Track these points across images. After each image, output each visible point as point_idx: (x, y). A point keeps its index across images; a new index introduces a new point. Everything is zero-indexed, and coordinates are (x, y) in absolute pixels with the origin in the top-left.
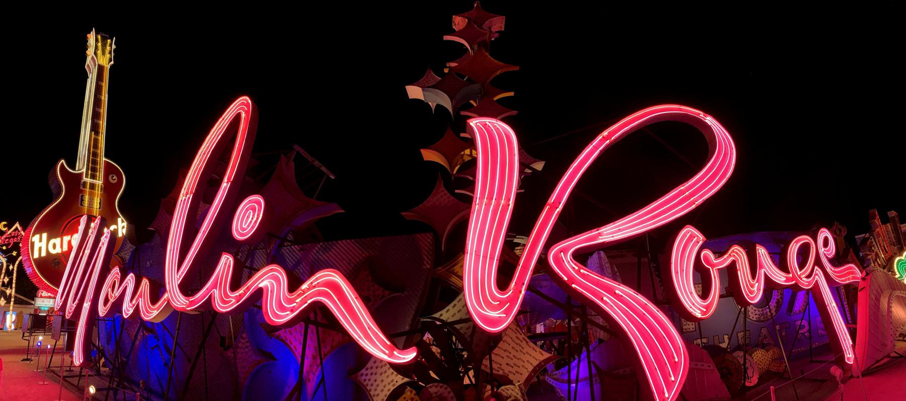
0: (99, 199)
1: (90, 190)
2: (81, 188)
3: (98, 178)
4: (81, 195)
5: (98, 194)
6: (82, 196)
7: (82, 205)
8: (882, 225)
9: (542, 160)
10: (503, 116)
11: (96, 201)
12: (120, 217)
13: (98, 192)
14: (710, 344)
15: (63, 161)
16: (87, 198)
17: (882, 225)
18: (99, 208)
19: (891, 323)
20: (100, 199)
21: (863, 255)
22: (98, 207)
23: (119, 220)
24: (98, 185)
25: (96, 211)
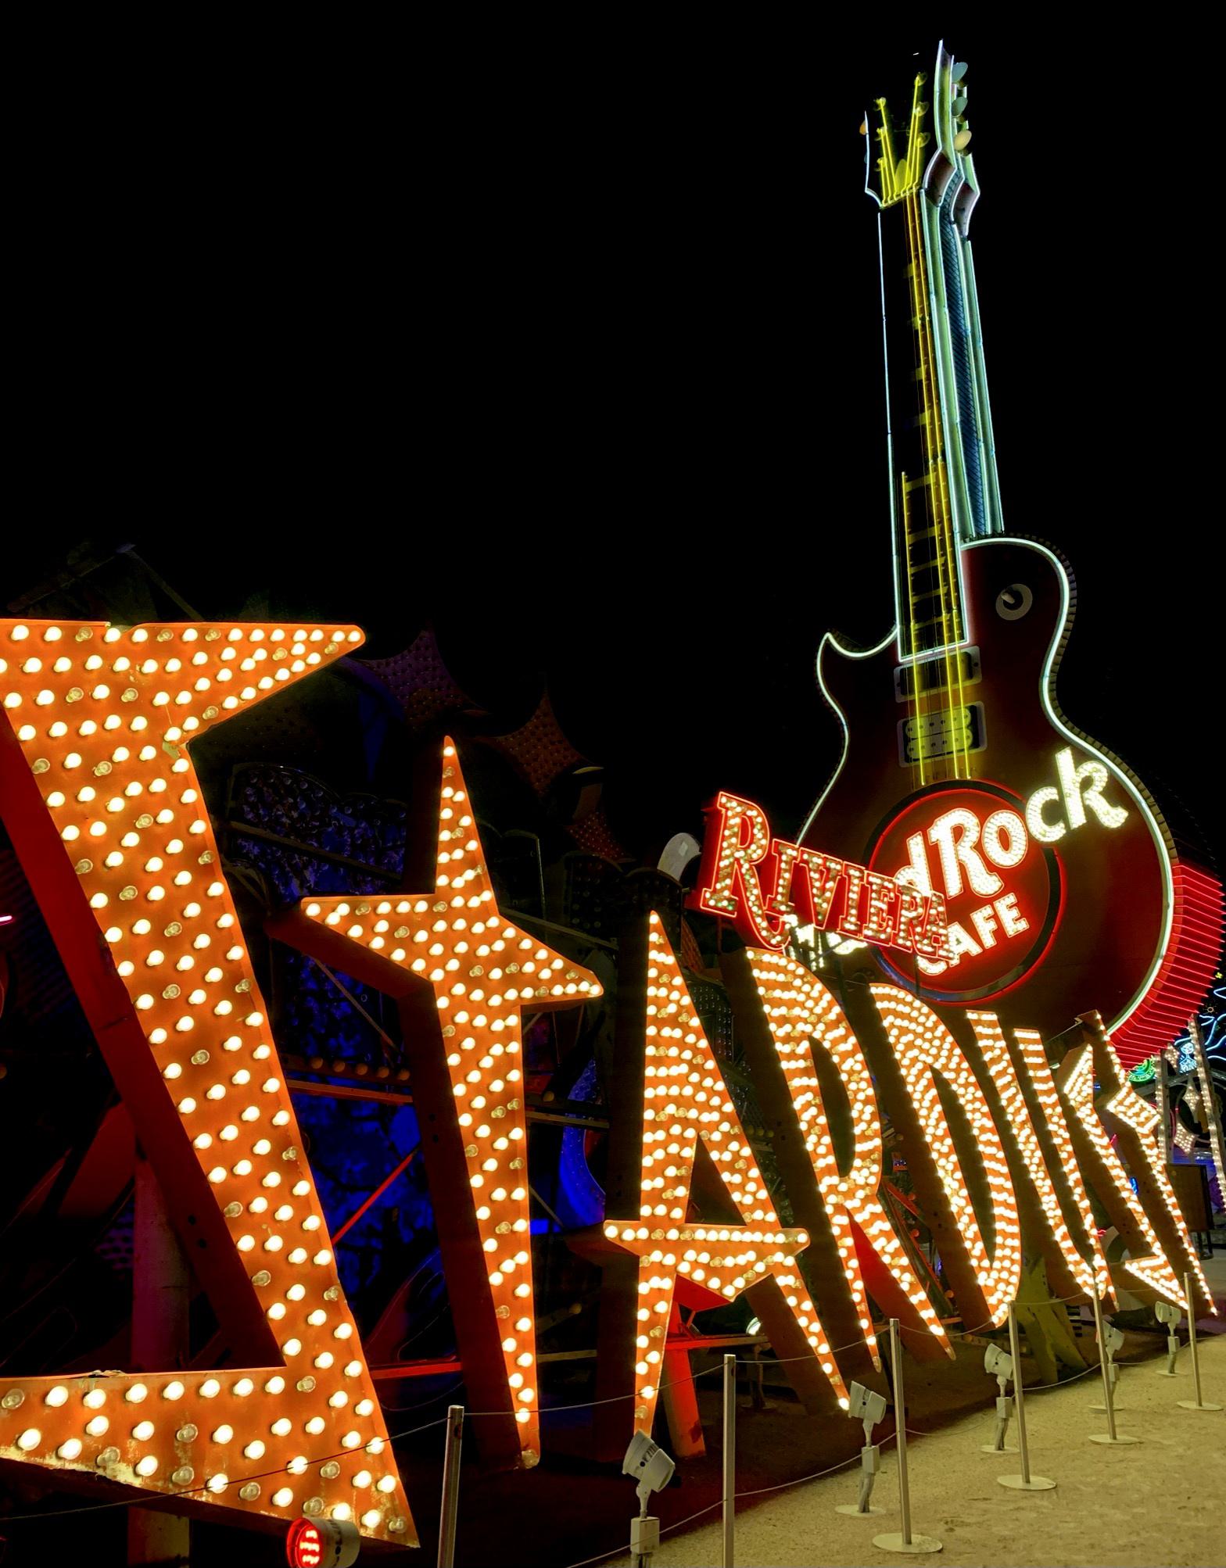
0: (964, 712)
1: (909, 698)
2: (900, 699)
3: (946, 635)
4: (900, 723)
5: (956, 692)
6: (905, 723)
7: (908, 759)
8: (527, 1012)
9: (421, 1544)
10: (484, 823)
11: (953, 725)
12: (1063, 742)
13: (959, 688)
14: (1038, 1189)
15: (828, 635)
16: (919, 724)
17: (527, 1012)
18: (975, 744)
19: (936, 1214)
20: (973, 710)
21: (729, 900)
22: (966, 744)
23: (1064, 759)
24: (954, 658)
25: (961, 760)
